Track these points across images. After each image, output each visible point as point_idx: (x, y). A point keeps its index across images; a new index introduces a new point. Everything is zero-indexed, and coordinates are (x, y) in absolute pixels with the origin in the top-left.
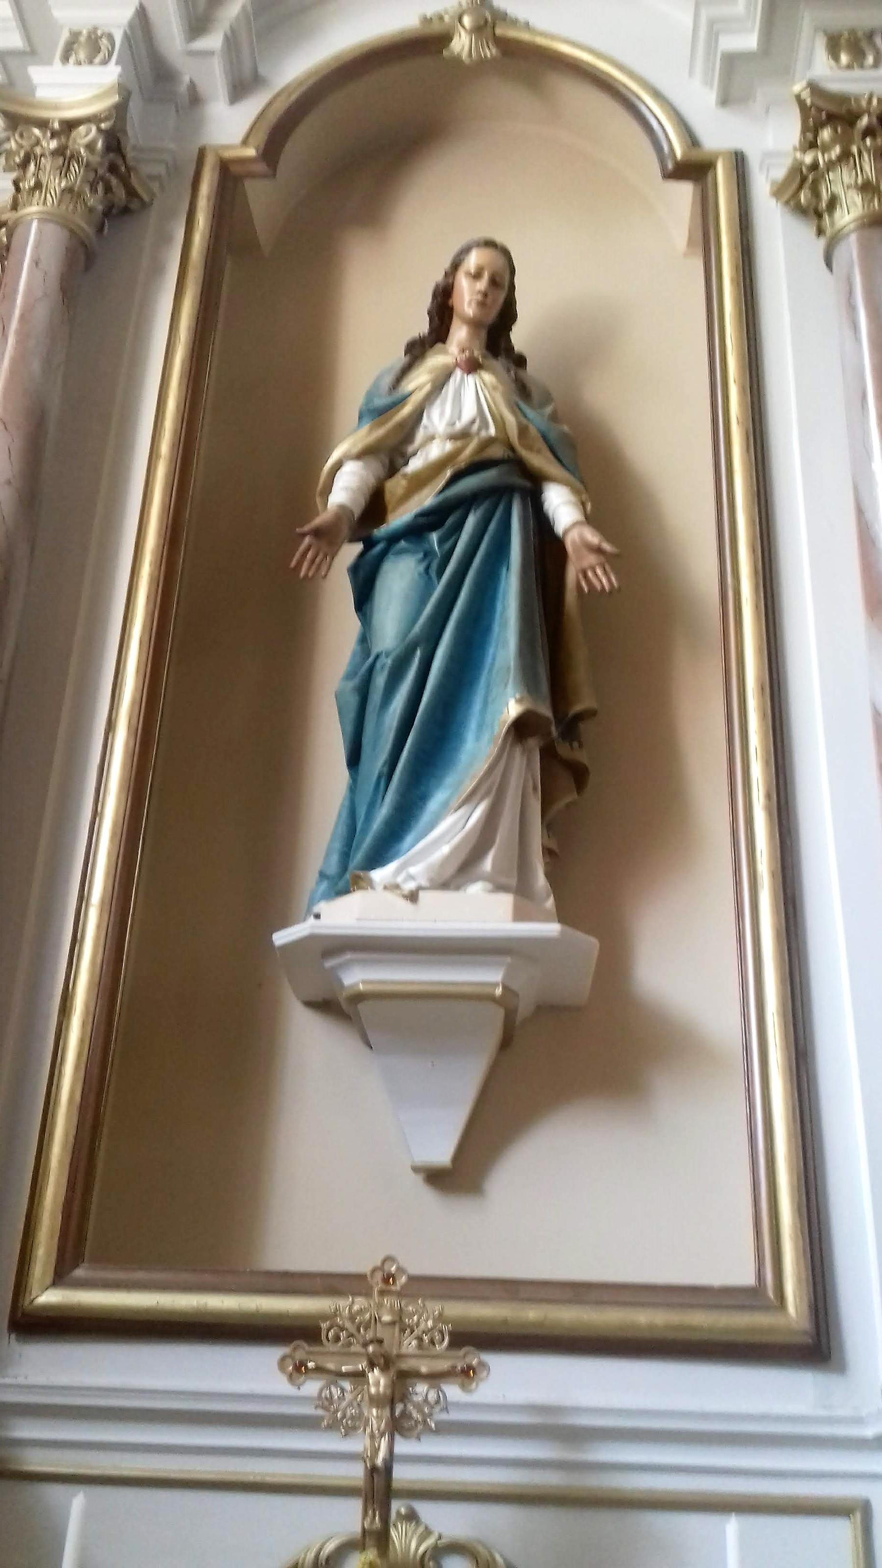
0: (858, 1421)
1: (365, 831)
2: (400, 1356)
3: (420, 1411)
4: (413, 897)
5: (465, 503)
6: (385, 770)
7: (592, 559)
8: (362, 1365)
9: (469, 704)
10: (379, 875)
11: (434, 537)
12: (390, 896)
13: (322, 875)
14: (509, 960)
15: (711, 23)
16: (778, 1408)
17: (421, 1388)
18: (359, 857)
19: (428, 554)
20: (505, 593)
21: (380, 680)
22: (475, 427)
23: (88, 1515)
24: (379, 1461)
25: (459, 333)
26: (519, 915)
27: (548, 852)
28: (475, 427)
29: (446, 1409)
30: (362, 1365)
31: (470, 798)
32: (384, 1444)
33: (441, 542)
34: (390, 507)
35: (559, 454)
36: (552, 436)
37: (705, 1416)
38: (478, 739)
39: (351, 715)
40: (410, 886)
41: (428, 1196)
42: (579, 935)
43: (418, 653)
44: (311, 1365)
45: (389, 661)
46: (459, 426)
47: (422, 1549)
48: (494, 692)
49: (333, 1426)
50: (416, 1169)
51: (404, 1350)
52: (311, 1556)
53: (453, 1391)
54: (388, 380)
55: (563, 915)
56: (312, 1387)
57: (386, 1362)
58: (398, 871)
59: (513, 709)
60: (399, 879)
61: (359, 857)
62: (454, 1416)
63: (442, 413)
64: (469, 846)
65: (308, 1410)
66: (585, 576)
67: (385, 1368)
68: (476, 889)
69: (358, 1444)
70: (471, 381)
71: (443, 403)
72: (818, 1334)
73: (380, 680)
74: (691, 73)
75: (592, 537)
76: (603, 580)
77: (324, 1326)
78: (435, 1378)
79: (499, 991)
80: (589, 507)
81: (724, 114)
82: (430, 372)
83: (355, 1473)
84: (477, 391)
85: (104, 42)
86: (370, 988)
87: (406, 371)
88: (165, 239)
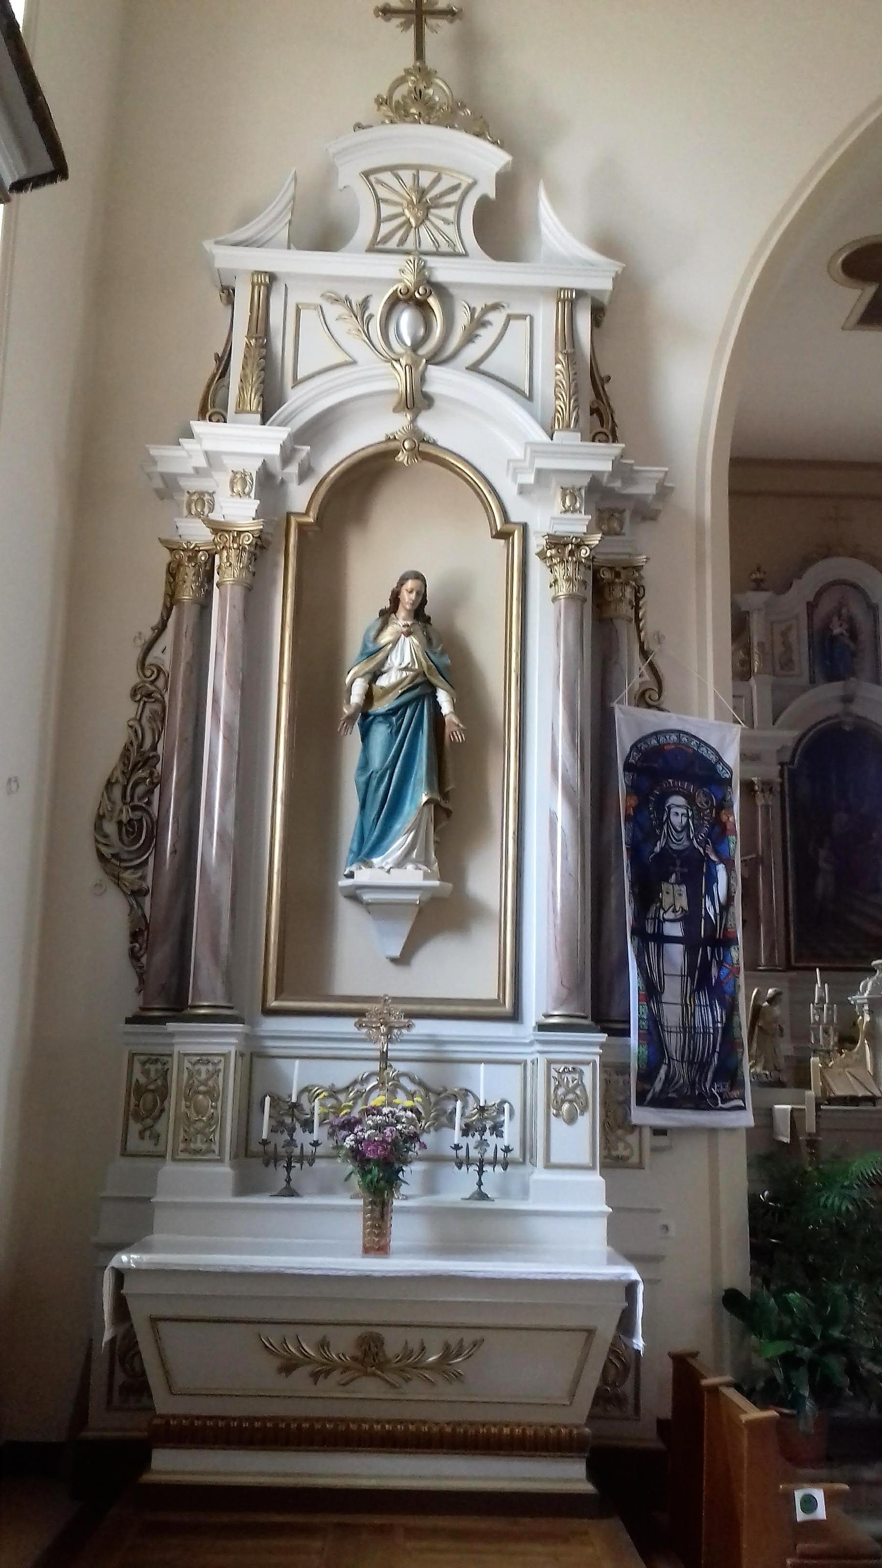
0: (525, 1038)
1: (369, 838)
2: (389, 1022)
3: (395, 1036)
4: (389, 871)
5: (404, 706)
6: (376, 817)
7: (456, 728)
8: (379, 1025)
9: (407, 789)
10: (376, 861)
11: (394, 719)
12: (380, 871)
13: (351, 851)
14: (421, 892)
15: (515, 469)
16: (502, 1034)
17: (395, 1031)
18: (366, 850)
19: (391, 724)
20: (421, 751)
21: (374, 782)
22: (410, 665)
23: (300, 1065)
24: (385, 1050)
25: (402, 613)
26: (426, 876)
27: (436, 842)
28: (410, 665)
29: (403, 1036)
30: (379, 1025)
31: (409, 831)
32: (386, 1045)
33: (397, 720)
34: (375, 699)
35: (444, 675)
36: (441, 667)
37: (499, 1037)
38: (411, 804)
39: (362, 792)
40: (388, 867)
41: (391, 966)
42: (447, 884)
43: (388, 772)
44: (364, 1025)
45: (378, 775)
46: (403, 666)
47: (394, 1074)
48: (417, 788)
49: (371, 1041)
50: (387, 958)
51: (391, 1020)
52: (360, 1078)
53: (404, 1031)
54: (373, 633)
55: (442, 879)
56: (364, 1030)
57: (385, 1024)
58: (383, 860)
59: (424, 799)
60: (383, 865)
61: (366, 850)
62: (405, 1038)
63: (397, 656)
64: (406, 851)
65: (363, 1037)
66: (452, 734)
67: (385, 1026)
68: (410, 867)
69: (378, 1046)
70: (407, 639)
71: (397, 652)
72: (515, 1014)
73: (374, 782)
74: (507, 475)
75: (455, 720)
76: (459, 738)
77: (367, 1014)
78: (399, 1028)
79: (418, 902)
80: (455, 700)
81: (519, 499)
82: (391, 635)
83: (378, 1054)
84: (411, 651)
85: (248, 478)
86: (374, 901)
87: (381, 630)
88: (276, 565)
